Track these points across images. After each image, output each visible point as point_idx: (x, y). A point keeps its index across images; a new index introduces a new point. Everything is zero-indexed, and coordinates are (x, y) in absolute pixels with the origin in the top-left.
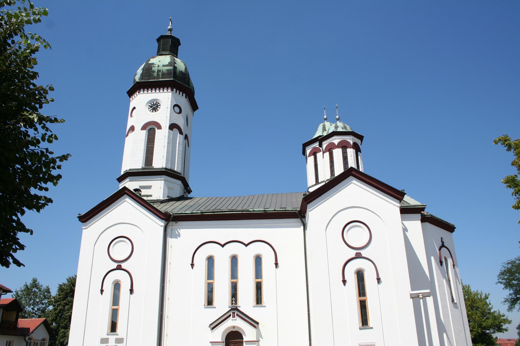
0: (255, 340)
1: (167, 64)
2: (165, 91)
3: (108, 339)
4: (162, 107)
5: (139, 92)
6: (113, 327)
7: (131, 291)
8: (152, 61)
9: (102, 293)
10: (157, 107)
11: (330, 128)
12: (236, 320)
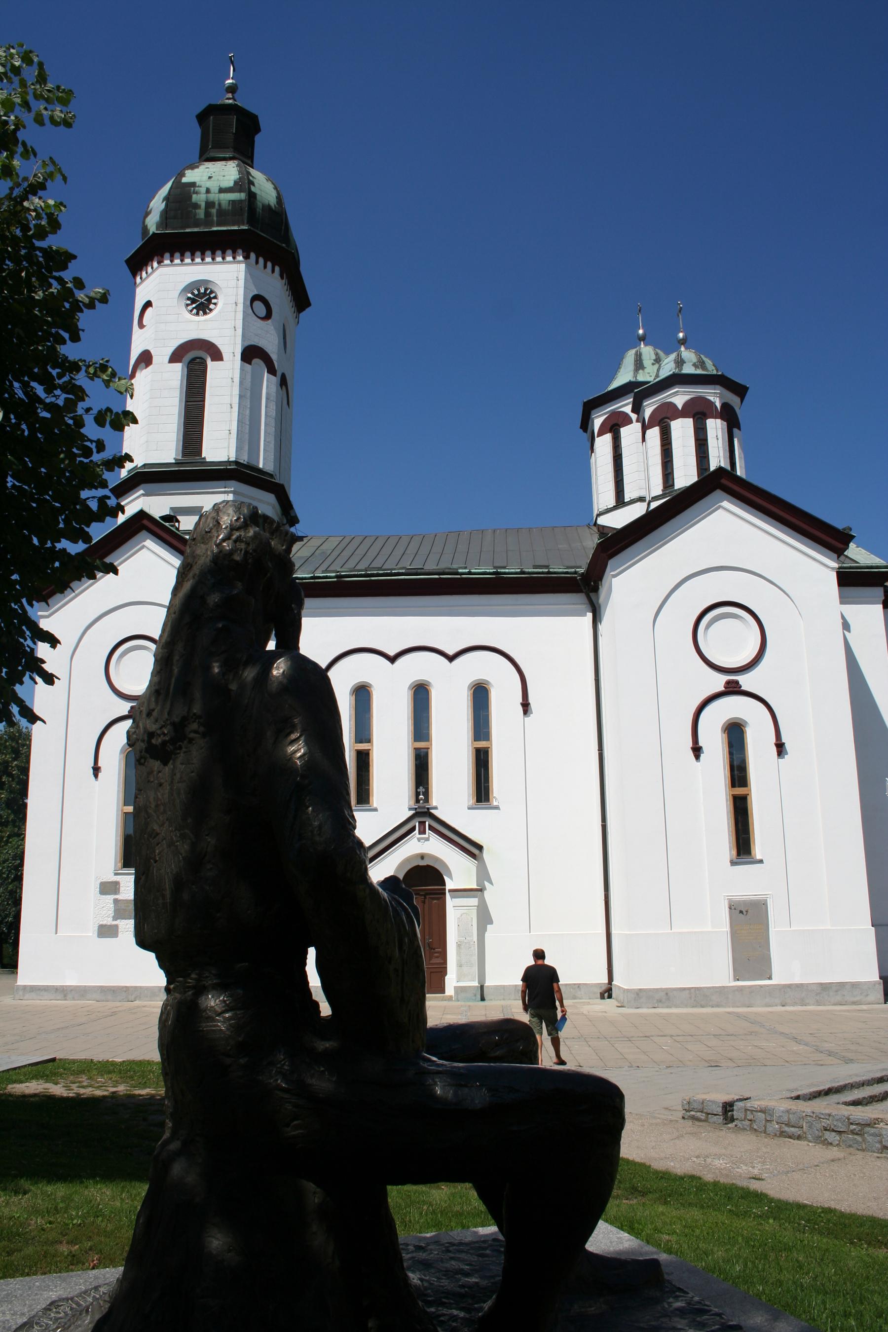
0: (475, 887)
1: (231, 184)
2: (229, 258)
3: (117, 884)
4: (221, 301)
5: (159, 263)
8: (190, 176)
9: (96, 776)
10: (209, 300)
12: (427, 839)
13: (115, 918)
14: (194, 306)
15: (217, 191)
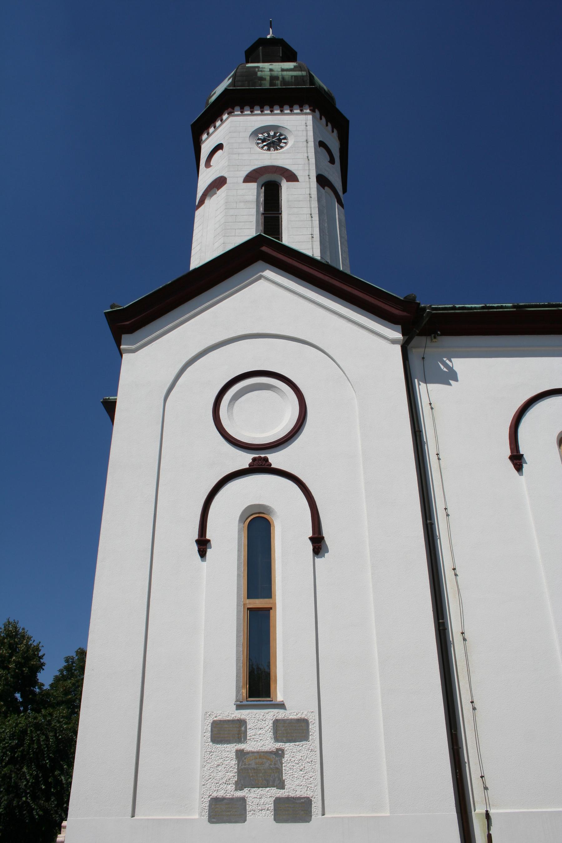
3: (242, 723)
4: (291, 141)
6: (258, 683)
7: (318, 543)
9: (202, 553)
10: (280, 140)
11: (442, 367)
13: (239, 786)
14: (265, 144)
15: (280, 70)
